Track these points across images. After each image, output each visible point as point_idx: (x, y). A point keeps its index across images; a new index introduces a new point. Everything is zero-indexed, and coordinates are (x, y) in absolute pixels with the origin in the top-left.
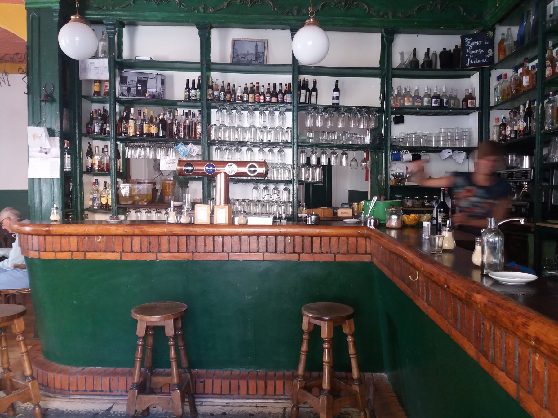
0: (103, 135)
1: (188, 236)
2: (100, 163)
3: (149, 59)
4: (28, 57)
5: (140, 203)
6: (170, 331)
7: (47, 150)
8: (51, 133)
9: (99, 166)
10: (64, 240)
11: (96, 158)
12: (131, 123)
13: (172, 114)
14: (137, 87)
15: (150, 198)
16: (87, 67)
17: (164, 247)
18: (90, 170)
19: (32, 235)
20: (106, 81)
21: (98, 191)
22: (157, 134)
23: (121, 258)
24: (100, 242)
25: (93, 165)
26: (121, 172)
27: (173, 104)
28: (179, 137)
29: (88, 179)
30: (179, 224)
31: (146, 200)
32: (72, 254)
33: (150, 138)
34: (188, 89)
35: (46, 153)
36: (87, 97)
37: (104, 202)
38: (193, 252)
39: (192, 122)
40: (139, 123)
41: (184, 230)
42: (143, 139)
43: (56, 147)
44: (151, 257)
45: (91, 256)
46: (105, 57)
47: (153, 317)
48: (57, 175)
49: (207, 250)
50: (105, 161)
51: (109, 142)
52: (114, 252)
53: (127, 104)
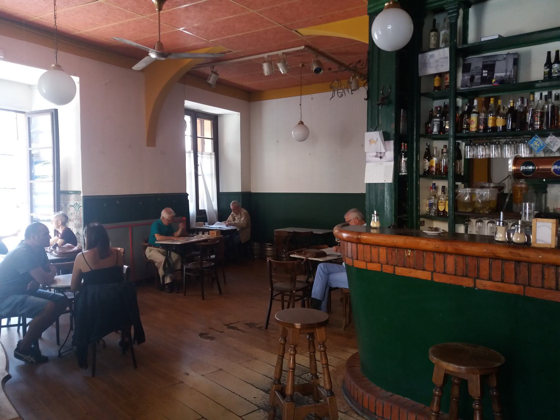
0: (442, 134)
1: (518, 262)
2: (438, 164)
3: (497, 37)
4: (369, 62)
5: (481, 212)
6: (475, 389)
7: (382, 155)
8: (386, 137)
9: (436, 169)
10: (374, 250)
11: (435, 159)
12: (474, 117)
13: (526, 100)
14: (482, 74)
15: (493, 205)
16: (427, 61)
17: (484, 272)
18: (428, 174)
19: (347, 242)
20: (447, 73)
21: (435, 196)
22: (504, 127)
23: (432, 278)
24: (409, 256)
25: (431, 167)
26: (462, 174)
27: (531, 86)
28: (533, 128)
29: (425, 184)
30: (509, 243)
31: (488, 208)
32: (382, 267)
33: (495, 134)
34: (549, 64)
35: (381, 157)
36: (426, 95)
37: (441, 208)
38: (525, 286)
39: (553, 107)
40: (482, 116)
41: (511, 253)
42: (489, 136)
43: (390, 150)
44: (467, 283)
45: (401, 271)
46: (446, 47)
47: (451, 365)
48: (389, 179)
49: (547, 284)
50: (443, 163)
51: (447, 141)
52: (424, 270)
53: (469, 95)
